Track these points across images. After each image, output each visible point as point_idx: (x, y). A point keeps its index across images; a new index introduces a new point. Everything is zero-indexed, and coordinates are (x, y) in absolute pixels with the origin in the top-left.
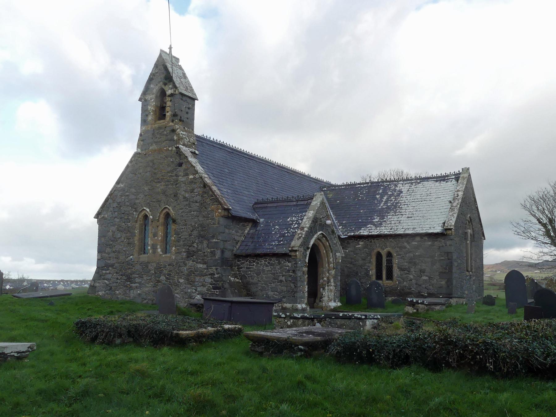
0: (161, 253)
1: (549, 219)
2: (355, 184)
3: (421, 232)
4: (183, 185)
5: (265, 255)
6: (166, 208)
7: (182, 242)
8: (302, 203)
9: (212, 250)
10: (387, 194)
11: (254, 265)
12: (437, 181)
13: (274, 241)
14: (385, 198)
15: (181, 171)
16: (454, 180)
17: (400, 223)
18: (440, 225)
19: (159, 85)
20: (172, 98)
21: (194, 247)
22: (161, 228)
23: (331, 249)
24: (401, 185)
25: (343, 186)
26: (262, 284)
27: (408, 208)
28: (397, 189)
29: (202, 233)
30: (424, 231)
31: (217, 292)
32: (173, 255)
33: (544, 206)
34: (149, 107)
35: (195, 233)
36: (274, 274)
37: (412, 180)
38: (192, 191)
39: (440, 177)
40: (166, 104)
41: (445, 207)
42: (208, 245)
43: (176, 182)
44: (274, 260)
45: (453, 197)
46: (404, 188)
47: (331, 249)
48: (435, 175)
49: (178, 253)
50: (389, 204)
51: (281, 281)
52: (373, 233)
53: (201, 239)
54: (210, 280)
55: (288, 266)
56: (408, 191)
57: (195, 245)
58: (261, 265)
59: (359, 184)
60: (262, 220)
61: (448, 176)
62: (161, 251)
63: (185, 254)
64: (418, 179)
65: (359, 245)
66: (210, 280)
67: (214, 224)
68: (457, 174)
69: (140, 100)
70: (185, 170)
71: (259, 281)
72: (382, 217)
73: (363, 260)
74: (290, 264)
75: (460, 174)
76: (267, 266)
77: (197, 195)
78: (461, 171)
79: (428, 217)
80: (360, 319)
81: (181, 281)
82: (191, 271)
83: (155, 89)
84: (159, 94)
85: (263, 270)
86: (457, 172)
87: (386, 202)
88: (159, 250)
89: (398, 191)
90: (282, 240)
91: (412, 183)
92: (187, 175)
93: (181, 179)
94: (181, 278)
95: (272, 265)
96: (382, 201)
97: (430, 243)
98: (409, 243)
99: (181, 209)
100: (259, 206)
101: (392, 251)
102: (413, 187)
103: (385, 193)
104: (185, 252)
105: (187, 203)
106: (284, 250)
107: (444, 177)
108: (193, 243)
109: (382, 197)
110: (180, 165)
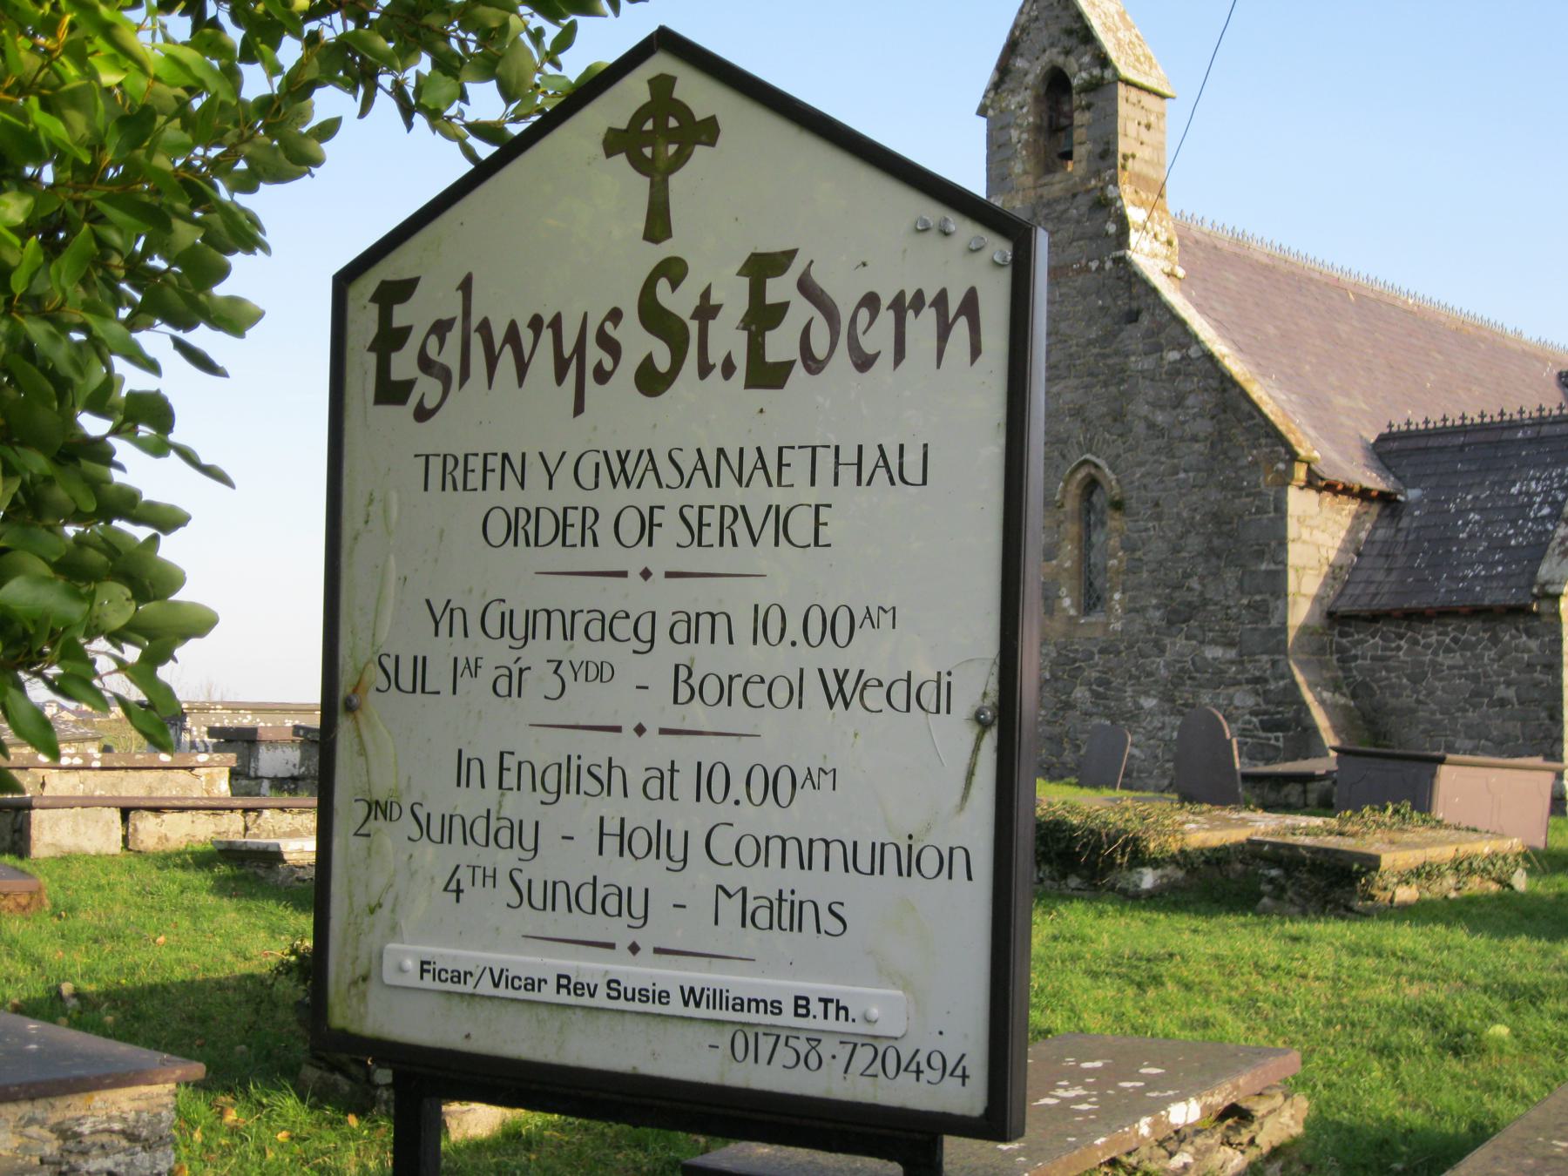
0: (1072, 612)
1: (123, 1132)
4: (1143, 384)
5: (1444, 614)
6: (1086, 462)
7: (1145, 575)
9: (1258, 598)
11: (1399, 648)
13: (1471, 565)
15: (1132, 337)
19: (1045, 58)
20: (1090, 98)
21: (1190, 589)
22: (1072, 529)
26: (1433, 713)
29: (1216, 542)
31: (1277, 739)
32: (1118, 619)
33: (1535, 1114)
34: (1014, 134)
35: (1194, 543)
36: (1475, 678)
38: (1178, 402)
40: (1071, 118)
42: (1241, 582)
43: (1119, 375)
44: (1474, 632)
49: (1132, 610)
51: (1503, 702)
53: (1214, 561)
54: (1250, 701)
55: (1529, 651)
57: (1194, 583)
58: (1427, 646)
60: (1413, 494)
62: (1072, 605)
63: (1158, 614)
66: (1250, 701)
67: (1260, 510)
69: (982, 111)
70: (1150, 334)
71: (1418, 701)
74: (1534, 644)
76: (1448, 650)
77: (1194, 417)
81: (1149, 703)
82: (1182, 670)
83: (1032, 69)
84: (1042, 91)
85: (1434, 664)
88: (1067, 602)
90: (1500, 562)
92: (1158, 348)
93: (1138, 363)
94: (1147, 694)
95: (1467, 646)
99: (1141, 464)
100: (1394, 445)
104: (1157, 607)
105: (1162, 442)
106: (1508, 597)
108: (1187, 576)
110: (1133, 317)
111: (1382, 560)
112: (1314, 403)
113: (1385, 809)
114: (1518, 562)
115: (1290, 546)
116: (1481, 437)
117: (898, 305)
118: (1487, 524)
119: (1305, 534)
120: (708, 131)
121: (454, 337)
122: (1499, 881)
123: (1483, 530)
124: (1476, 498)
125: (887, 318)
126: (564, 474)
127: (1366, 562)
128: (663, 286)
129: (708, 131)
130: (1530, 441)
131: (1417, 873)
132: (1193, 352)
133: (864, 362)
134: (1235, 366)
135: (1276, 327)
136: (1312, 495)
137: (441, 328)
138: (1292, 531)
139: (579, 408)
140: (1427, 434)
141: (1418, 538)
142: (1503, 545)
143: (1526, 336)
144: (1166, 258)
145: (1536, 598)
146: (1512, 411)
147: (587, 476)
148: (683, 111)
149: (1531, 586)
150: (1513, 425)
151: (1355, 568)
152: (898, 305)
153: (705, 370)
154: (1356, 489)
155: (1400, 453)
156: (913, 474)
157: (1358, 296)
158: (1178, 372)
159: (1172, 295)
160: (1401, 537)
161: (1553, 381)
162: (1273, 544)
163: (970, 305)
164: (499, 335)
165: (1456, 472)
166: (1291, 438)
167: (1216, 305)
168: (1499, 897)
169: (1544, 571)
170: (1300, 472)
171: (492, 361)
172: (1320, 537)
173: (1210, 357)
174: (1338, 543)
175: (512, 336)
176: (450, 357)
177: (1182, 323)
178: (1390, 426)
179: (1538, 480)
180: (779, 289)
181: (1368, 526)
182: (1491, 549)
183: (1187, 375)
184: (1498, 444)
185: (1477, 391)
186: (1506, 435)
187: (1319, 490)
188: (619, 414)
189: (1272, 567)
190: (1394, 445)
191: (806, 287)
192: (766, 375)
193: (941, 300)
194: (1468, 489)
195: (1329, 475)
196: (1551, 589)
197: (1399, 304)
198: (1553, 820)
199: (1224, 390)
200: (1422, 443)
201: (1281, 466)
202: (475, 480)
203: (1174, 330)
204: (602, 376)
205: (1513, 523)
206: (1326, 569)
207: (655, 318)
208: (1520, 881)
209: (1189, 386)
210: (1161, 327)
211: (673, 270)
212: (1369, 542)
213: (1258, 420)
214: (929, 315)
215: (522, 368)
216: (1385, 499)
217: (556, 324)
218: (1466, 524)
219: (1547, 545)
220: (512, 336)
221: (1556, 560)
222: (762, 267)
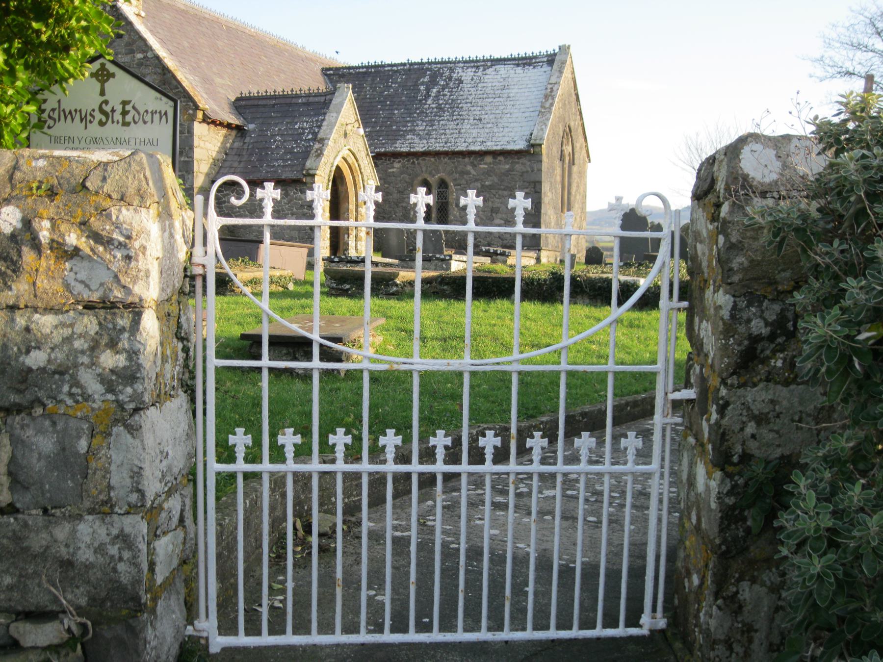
2: (383, 66)
3: (495, 148)
8: (317, 99)
10: (437, 84)
12: (518, 65)
13: (277, 160)
14: (435, 90)
16: (545, 65)
17: (459, 133)
18: (524, 138)
23: (361, 173)
24: (460, 71)
25: (362, 67)
27: (472, 109)
28: (455, 76)
30: (499, 148)
37: (477, 61)
39: (523, 59)
41: (532, 109)
45: (544, 92)
46: (467, 75)
47: (361, 173)
48: (515, 55)
50: (441, 102)
52: (417, 149)
56: (472, 79)
59: (389, 65)
60: (251, 127)
61: (536, 57)
64: (488, 60)
65: (393, 167)
68: (551, 55)
70: (128, 44)
72: (431, 123)
73: (399, 192)
75: (555, 54)
78: (557, 50)
79: (506, 125)
80: (443, 260)
86: (551, 51)
87: (437, 97)
89: (456, 80)
90: (289, 159)
91: (478, 67)
92: (132, 52)
96: (430, 96)
97: (507, 167)
98: (474, 166)
100: (243, 103)
101: (448, 179)
102: (480, 73)
103: (433, 82)
107: (531, 58)
109: (428, 90)
111: (236, 157)
112: (206, 81)
113: (238, 260)
114: (297, 159)
115: (195, 150)
116: (282, 101)
117: (152, 113)
118: (285, 141)
119: (202, 144)
120: (113, 75)
121: (57, 112)
122: (283, 287)
123: (282, 144)
124: (280, 129)
125: (150, 115)
126: (83, 141)
127: (229, 158)
128: (104, 106)
129: (113, 75)
130: (304, 104)
131: (251, 282)
132: (149, 55)
133: (145, 122)
134: (170, 62)
135: (189, 43)
136: (205, 125)
137: (53, 110)
138: (196, 143)
139: (86, 128)
140: (258, 98)
141: (253, 147)
142: (291, 152)
143: (307, 49)
144: (136, 6)
145: (305, 176)
146: (296, 90)
147: (88, 141)
148: (108, 71)
149: (302, 170)
150: (297, 96)
151: (225, 161)
152: (152, 112)
153: (113, 122)
154: (226, 123)
155: (245, 107)
156: (155, 143)
157: (228, 27)
158: (142, 64)
159: (140, 26)
160: (246, 147)
161: (319, 72)
162: (187, 148)
163: (166, 113)
164: (67, 113)
165: (271, 117)
166: (196, 99)
167: (160, 31)
168: (283, 292)
169: (309, 164)
170: (200, 115)
171: (66, 118)
172: (209, 146)
173: (157, 57)
174: (217, 149)
175: (70, 112)
176: (56, 116)
177: (144, 40)
178: (241, 93)
179: (307, 122)
180: (128, 108)
181: (231, 141)
182: (285, 153)
183: (147, 66)
184: (290, 105)
185: (282, 76)
186: (294, 101)
187: (208, 124)
188: (94, 129)
189: (186, 159)
190: (243, 103)
191: (134, 107)
192: (126, 124)
193: (160, 112)
194: (276, 125)
195: (214, 117)
196: (311, 172)
197: (247, 31)
198: (308, 272)
199: (164, 74)
200: (256, 102)
201: (191, 112)
202: (62, 141)
203: (141, 43)
204: (91, 122)
205: (296, 141)
206: (211, 160)
207: (102, 111)
208: (291, 287)
209: (147, 71)
210: (134, 42)
211: (106, 102)
212: (231, 148)
213: (180, 89)
214: (158, 115)
215: (73, 120)
216: (239, 128)
217: (80, 111)
218: (275, 141)
219: (310, 152)
220: (70, 112)
221: (313, 159)
222: (125, 103)
